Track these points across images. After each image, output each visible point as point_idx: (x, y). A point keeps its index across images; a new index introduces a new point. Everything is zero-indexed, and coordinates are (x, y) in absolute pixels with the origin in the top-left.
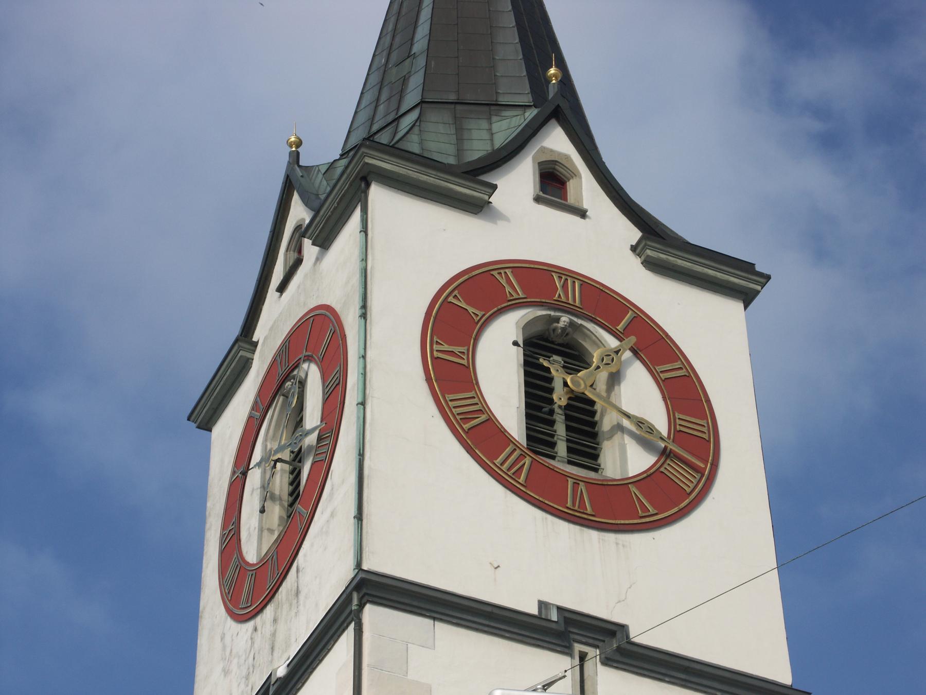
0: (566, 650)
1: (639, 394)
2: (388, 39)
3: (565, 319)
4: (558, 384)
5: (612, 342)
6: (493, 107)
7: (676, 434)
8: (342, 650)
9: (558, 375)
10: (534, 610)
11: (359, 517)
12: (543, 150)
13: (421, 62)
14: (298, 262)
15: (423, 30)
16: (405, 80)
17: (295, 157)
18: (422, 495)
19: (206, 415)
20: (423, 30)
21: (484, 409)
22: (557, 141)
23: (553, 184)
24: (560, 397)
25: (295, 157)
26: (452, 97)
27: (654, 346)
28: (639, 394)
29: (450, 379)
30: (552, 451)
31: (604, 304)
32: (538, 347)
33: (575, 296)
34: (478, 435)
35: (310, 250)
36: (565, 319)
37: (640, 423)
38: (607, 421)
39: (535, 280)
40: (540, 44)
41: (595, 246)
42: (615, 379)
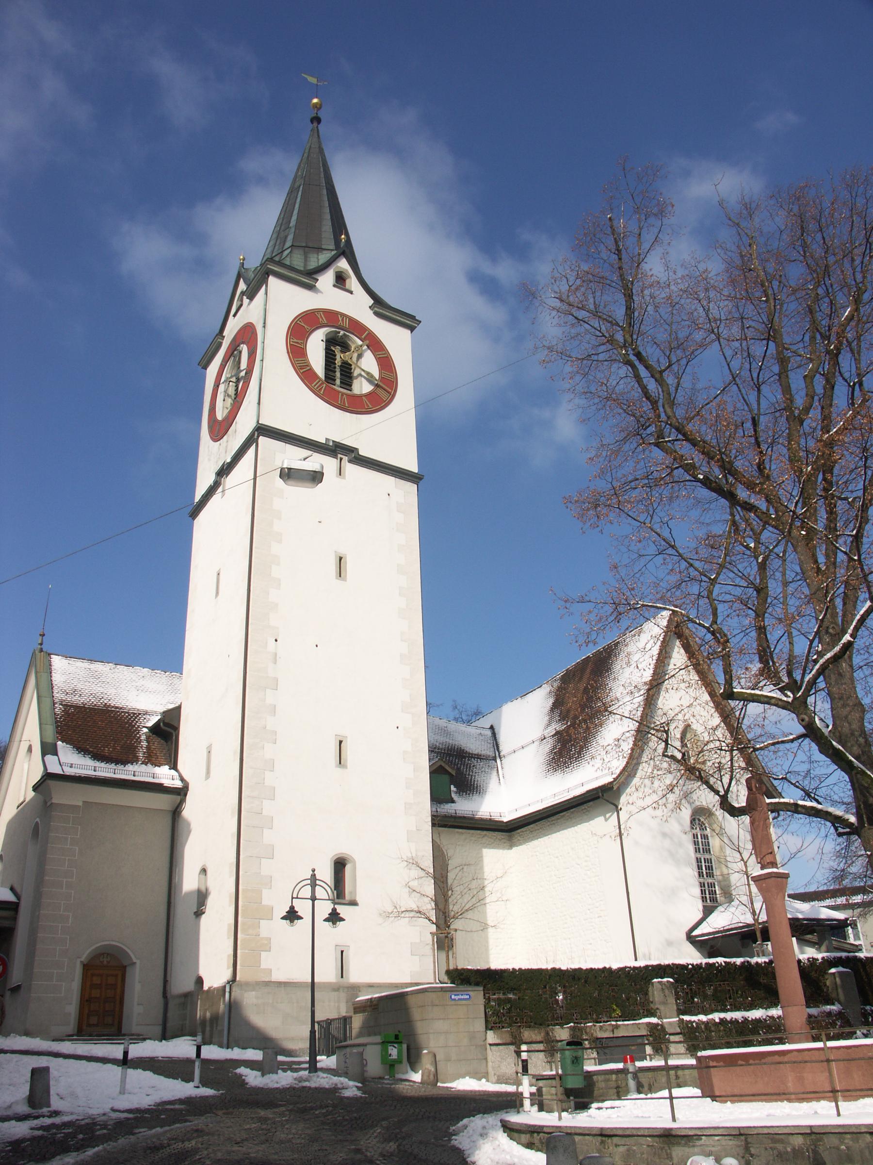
1: (369, 363)
3: (342, 332)
5: (360, 342)
11: (259, 403)
12: (338, 267)
13: (293, 230)
15: (294, 218)
16: (286, 237)
18: (283, 395)
20: (294, 218)
21: (309, 365)
23: (340, 280)
24: (338, 362)
26: (304, 245)
27: (375, 345)
28: (369, 363)
29: (297, 353)
30: (335, 382)
31: (357, 327)
32: (331, 342)
34: (306, 374)
35: (246, 301)
36: (342, 332)
38: (356, 372)
39: (332, 317)
40: (339, 225)
41: (355, 305)
42: (360, 356)
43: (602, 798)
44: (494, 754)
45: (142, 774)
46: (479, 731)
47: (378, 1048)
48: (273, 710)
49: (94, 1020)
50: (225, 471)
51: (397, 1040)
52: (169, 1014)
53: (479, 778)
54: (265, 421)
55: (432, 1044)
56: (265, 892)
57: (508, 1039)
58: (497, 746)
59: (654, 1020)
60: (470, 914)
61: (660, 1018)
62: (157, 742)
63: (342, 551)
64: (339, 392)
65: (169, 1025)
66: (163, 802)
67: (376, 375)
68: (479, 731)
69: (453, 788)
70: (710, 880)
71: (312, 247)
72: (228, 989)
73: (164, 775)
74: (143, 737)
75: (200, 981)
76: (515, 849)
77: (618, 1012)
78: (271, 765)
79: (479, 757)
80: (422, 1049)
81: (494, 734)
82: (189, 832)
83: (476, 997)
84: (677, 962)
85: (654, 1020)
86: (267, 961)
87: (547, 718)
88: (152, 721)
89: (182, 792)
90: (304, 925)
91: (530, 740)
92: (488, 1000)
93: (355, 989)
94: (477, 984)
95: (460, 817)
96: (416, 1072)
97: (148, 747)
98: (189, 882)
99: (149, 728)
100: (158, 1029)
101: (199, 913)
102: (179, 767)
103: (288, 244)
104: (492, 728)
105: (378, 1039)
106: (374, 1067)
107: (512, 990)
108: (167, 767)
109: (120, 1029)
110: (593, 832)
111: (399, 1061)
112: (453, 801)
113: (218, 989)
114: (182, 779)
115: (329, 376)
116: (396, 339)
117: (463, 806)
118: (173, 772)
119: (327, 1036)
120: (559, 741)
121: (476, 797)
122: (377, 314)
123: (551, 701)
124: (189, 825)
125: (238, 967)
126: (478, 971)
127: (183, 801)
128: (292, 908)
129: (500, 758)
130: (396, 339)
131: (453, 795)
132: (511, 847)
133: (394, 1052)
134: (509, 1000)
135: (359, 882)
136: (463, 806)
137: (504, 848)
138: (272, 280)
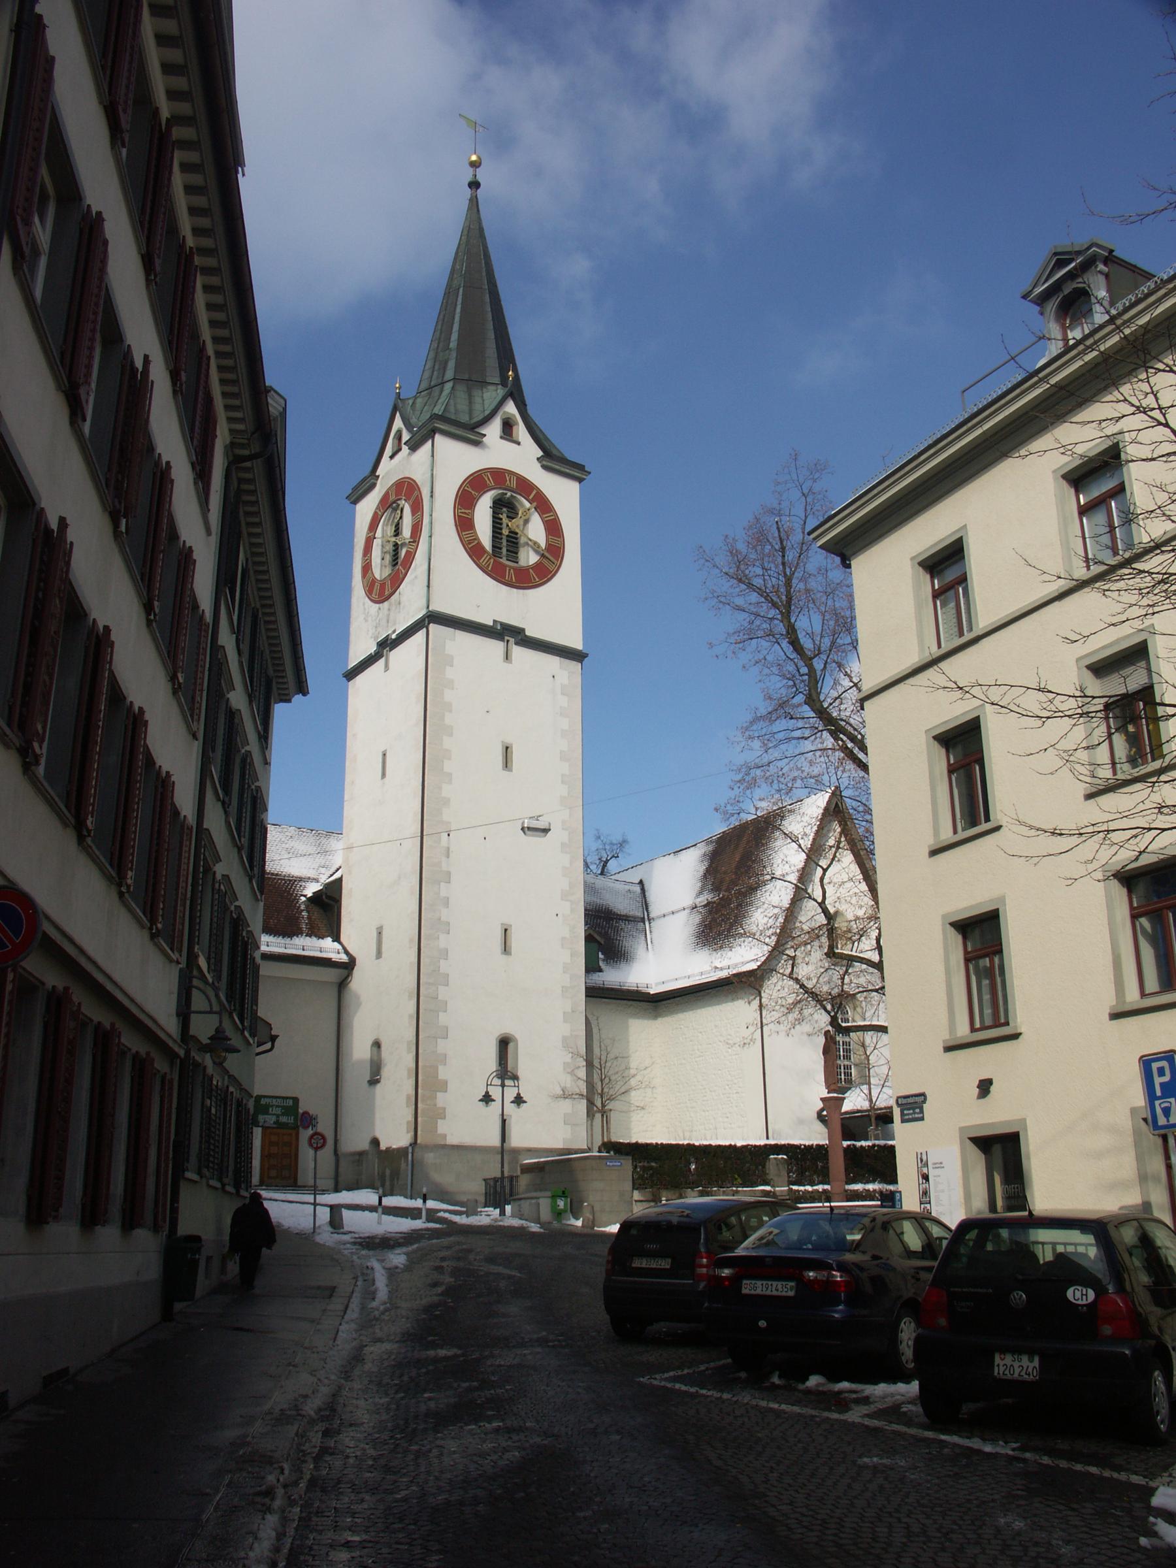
0: (502, 639)
1: (536, 530)
2: (438, 333)
3: (509, 494)
4: (504, 525)
5: (527, 505)
6: (483, 384)
7: (549, 547)
8: (420, 636)
9: (505, 520)
10: (491, 624)
11: (428, 587)
12: (505, 413)
13: (454, 354)
14: (400, 449)
15: (455, 336)
16: (446, 363)
17: (557, 1097)
18: (451, 576)
19: (357, 496)
20: (455, 336)
21: (477, 538)
22: (511, 408)
23: (508, 429)
24: (505, 532)
25: (557, 1097)
26: (466, 377)
27: (543, 505)
28: (536, 530)
29: (464, 524)
30: (503, 560)
31: (525, 486)
32: (499, 505)
33: (514, 485)
34: (475, 551)
35: (405, 449)
36: (509, 494)
37: (535, 543)
38: (523, 540)
39: (499, 476)
40: (506, 357)
41: (521, 457)
42: (526, 522)
43: (745, 984)
44: (641, 919)
45: (313, 949)
46: (627, 887)
47: (549, 1200)
48: (446, 902)
49: (273, 1173)
50: (387, 645)
51: (564, 1195)
52: (341, 1170)
53: (627, 943)
54: (436, 606)
55: (591, 1198)
56: (441, 1068)
57: (649, 1197)
58: (646, 906)
59: (768, 1188)
60: (622, 1098)
61: (773, 1186)
62: (317, 913)
63: (509, 740)
64: (506, 566)
65: (340, 1179)
66: (332, 975)
67: (543, 545)
68: (627, 887)
69: (601, 956)
70: (846, 1063)
71: (472, 381)
72: (410, 1150)
73: (327, 948)
74: (303, 907)
75: (375, 1142)
76: (660, 1020)
77: (739, 1180)
78: (444, 954)
79: (627, 918)
80: (582, 1202)
81: (643, 890)
82: (359, 1005)
83: (627, 1164)
84: (792, 1142)
85: (768, 1188)
86: (443, 1127)
87: (699, 884)
88: (311, 889)
89: (350, 965)
90: (495, 1107)
91: (681, 907)
92: (635, 1167)
93: (516, 1152)
94: (627, 1154)
95: (608, 989)
96: (577, 1219)
97: (309, 918)
98: (359, 1049)
99: (310, 899)
100: (331, 1183)
101: (374, 1082)
102: (342, 939)
103: (449, 374)
104: (641, 882)
105: (549, 1194)
106: (546, 1214)
107: (655, 1160)
108: (329, 939)
109: (296, 1179)
110: (737, 1013)
111: (565, 1211)
112: (601, 970)
113: (398, 1150)
114: (347, 952)
115: (496, 546)
116: (564, 495)
117: (611, 976)
118: (336, 945)
119: (499, 1193)
120: (710, 912)
121: (623, 965)
122: (545, 467)
123: (702, 868)
124: (358, 997)
125: (419, 1132)
126: (629, 1144)
127: (350, 974)
128: (487, 1093)
129: (649, 920)
130: (564, 495)
131: (601, 963)
132: (656, 1017)
133: (561, 1204)
134: (651, 1168)
135: (524, 1062)
136: (611, 976)
137: (649, 1018)
138: (438, 437)
